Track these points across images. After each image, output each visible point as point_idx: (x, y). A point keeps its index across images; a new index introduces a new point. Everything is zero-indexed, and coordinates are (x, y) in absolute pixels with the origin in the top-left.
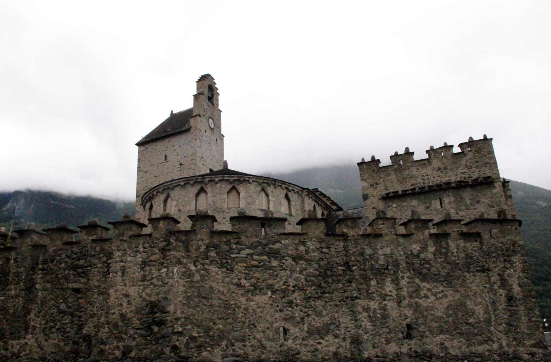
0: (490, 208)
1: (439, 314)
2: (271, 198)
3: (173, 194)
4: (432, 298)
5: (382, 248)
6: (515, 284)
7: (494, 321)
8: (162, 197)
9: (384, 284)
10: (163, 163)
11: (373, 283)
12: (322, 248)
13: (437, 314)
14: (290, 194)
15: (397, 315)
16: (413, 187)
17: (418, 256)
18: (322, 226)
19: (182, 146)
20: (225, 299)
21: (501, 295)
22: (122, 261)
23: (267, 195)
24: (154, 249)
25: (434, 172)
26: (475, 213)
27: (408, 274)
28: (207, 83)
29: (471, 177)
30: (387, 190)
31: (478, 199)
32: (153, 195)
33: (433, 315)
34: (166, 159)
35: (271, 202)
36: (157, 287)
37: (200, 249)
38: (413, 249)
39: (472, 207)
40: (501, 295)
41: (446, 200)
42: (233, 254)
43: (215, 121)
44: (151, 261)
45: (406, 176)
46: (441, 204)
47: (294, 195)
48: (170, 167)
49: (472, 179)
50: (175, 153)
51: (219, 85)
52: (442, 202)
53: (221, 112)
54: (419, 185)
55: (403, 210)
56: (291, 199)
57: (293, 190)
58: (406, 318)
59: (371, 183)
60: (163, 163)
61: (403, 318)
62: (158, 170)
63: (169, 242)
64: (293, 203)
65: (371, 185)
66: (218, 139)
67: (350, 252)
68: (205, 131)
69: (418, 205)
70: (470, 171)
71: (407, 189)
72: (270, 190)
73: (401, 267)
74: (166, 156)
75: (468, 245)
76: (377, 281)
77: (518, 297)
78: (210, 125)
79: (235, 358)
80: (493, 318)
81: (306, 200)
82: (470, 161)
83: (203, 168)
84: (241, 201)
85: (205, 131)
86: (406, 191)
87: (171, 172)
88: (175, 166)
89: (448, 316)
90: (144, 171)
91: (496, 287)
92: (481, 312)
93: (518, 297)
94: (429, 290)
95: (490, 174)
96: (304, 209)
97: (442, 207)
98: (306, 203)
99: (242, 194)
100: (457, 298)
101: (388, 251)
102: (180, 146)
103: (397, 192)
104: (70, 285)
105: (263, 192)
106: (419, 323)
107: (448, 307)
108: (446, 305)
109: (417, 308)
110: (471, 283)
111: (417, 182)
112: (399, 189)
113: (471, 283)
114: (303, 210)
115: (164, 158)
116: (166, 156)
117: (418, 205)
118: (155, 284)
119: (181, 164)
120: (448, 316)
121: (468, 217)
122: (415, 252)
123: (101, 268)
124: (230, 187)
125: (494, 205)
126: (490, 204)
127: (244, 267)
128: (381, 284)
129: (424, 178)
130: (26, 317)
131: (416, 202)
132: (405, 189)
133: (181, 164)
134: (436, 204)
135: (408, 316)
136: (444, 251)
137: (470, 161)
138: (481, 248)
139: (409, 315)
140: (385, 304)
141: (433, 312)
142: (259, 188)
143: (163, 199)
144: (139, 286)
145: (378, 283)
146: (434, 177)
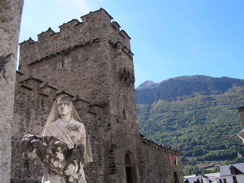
18: (28, 97)
20: (97, 142)
25: (61, 41)
31: (87, 57)
41: (66, 61)
46: (63, 65)
49: (85, 42)
52: (64, 63)
53: (130, 39)
54: (50, 52)
55: (39, 73)
65: (24, 58)
70: (85, 36)
79: (110, 165)
82: (86, 29)
97: (63, 67)
111: (50, 50)
117: (49, 68)
121: (78, 72)
125: (98, 60)
131: (48, 66)
134: (59, 65)
137: (86, 29)
146: (61, 45)
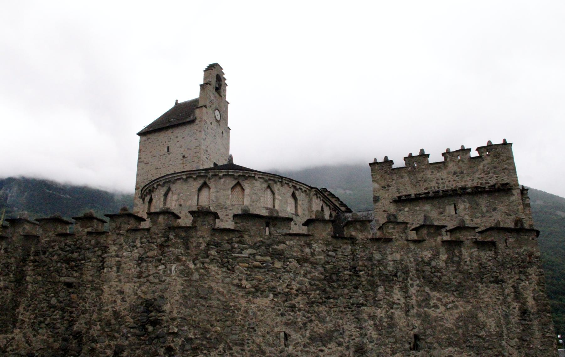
0: (506, 216)
1: (449, 325)
2: (277, 196)
3: (174, 187)
4: (442, 308)
5: (392, 254)
6: (530, 297)
7: (506, 335)
8: (163, 191)
9: (392, 291)
10: (165, 154)
11: (381, 289)
12: (329, 251)
13: (447, 325)
14: (297, 193)
15: (405, 324)
16: (426, 191)
17: (429, 264)
19: (186, 138)
21: (514, 308)
22: (117, 256)
23: (273, 193)
24: (152, 245)
26: (490, 221)
27: (418, 282)
28: (214, 72)
29: (488, 183)
30: (399, 193)
32: (154, 187)
33: (442, 326)
34: (168, 151)
35: (276, 201)
36: (153, 285)
37: (200, 246)
38: (424, 256)
39: (488, 215)
40: (514, 308)
42: (235, 253)
43: (221, 113)
44: (148, 257)
45: (419, 179)
46: (456, 210)
47: (302, 194)
48: (172, 159)
50: (178, 145)
51: (228, 75)
56: (298, 198)
57: (301, 189)
58: (414, 328)
59: (383, 185)
60: (165, 154)
61: (411, 328)
62: (160, 162)
63: (168, 238)
64: (300, 202)
66: (224, 132)
67: (357, 256)
68: (211, 123)
69: (431, 210)
71: (420, 192)
72: (276, 187)
73: (410, 274)
74: (168, 148)
75: (482, 254)
76: (385, 288)
77: (532, 311)
78: (217, 116)
80: (505, 332)
81: (313, 200)
83: (207, 162)
84: (245, 198)
85: (211, 123)
86: (420, 194)
87: (173, 164)
88: (177, 159)
89: (458, 328)
90: (145, 162)
91: (509, 299)
92: (493, 325)
93: (532, 311)
94: (439, 299)
95: (508, 180)
96: (311, 209)
97: (456, 213)
98: (313, 202)
99: (247, 191)
100: (468, 309)
101: (397, 256)
102: (183, 138)
103: (410, 195)
104: (62, 279)
105: (269, 190)
106: (427, 333)
107: (458, 318)
108: (457, 316)
109: (425, 318)
110: (483, 294)
112: (412, 192)
113: (483, 294)
114: (310, 210)
115: (166, 149)
116: (168, 148)
117: (431, 210)
118: (152, 281)
119: (184, 157)
120: (458, 328)
121: (483, 224)
122: (426, 259)
123: (96, 262)
124: (234, 182)
125: (511, 213)
126: (507, 212)
127: (246, 267)
128: (389, 291)
129: (438, 181)
130: (15, 310)
132: (418, 193)
133: (184, 157)
135: (416, 326)
136: (456, 259)
138: (495, 258)
139: (417, 325)
140: (392, 313)
141: (442, 323)
142: (265, 185)
143: (163, 193)
144: (135, 283)
145: (386, 290)
